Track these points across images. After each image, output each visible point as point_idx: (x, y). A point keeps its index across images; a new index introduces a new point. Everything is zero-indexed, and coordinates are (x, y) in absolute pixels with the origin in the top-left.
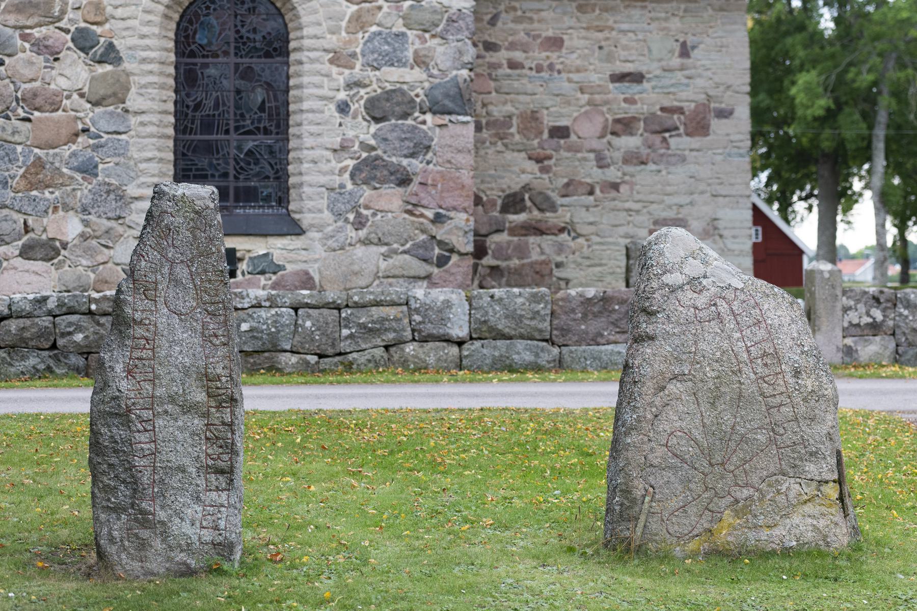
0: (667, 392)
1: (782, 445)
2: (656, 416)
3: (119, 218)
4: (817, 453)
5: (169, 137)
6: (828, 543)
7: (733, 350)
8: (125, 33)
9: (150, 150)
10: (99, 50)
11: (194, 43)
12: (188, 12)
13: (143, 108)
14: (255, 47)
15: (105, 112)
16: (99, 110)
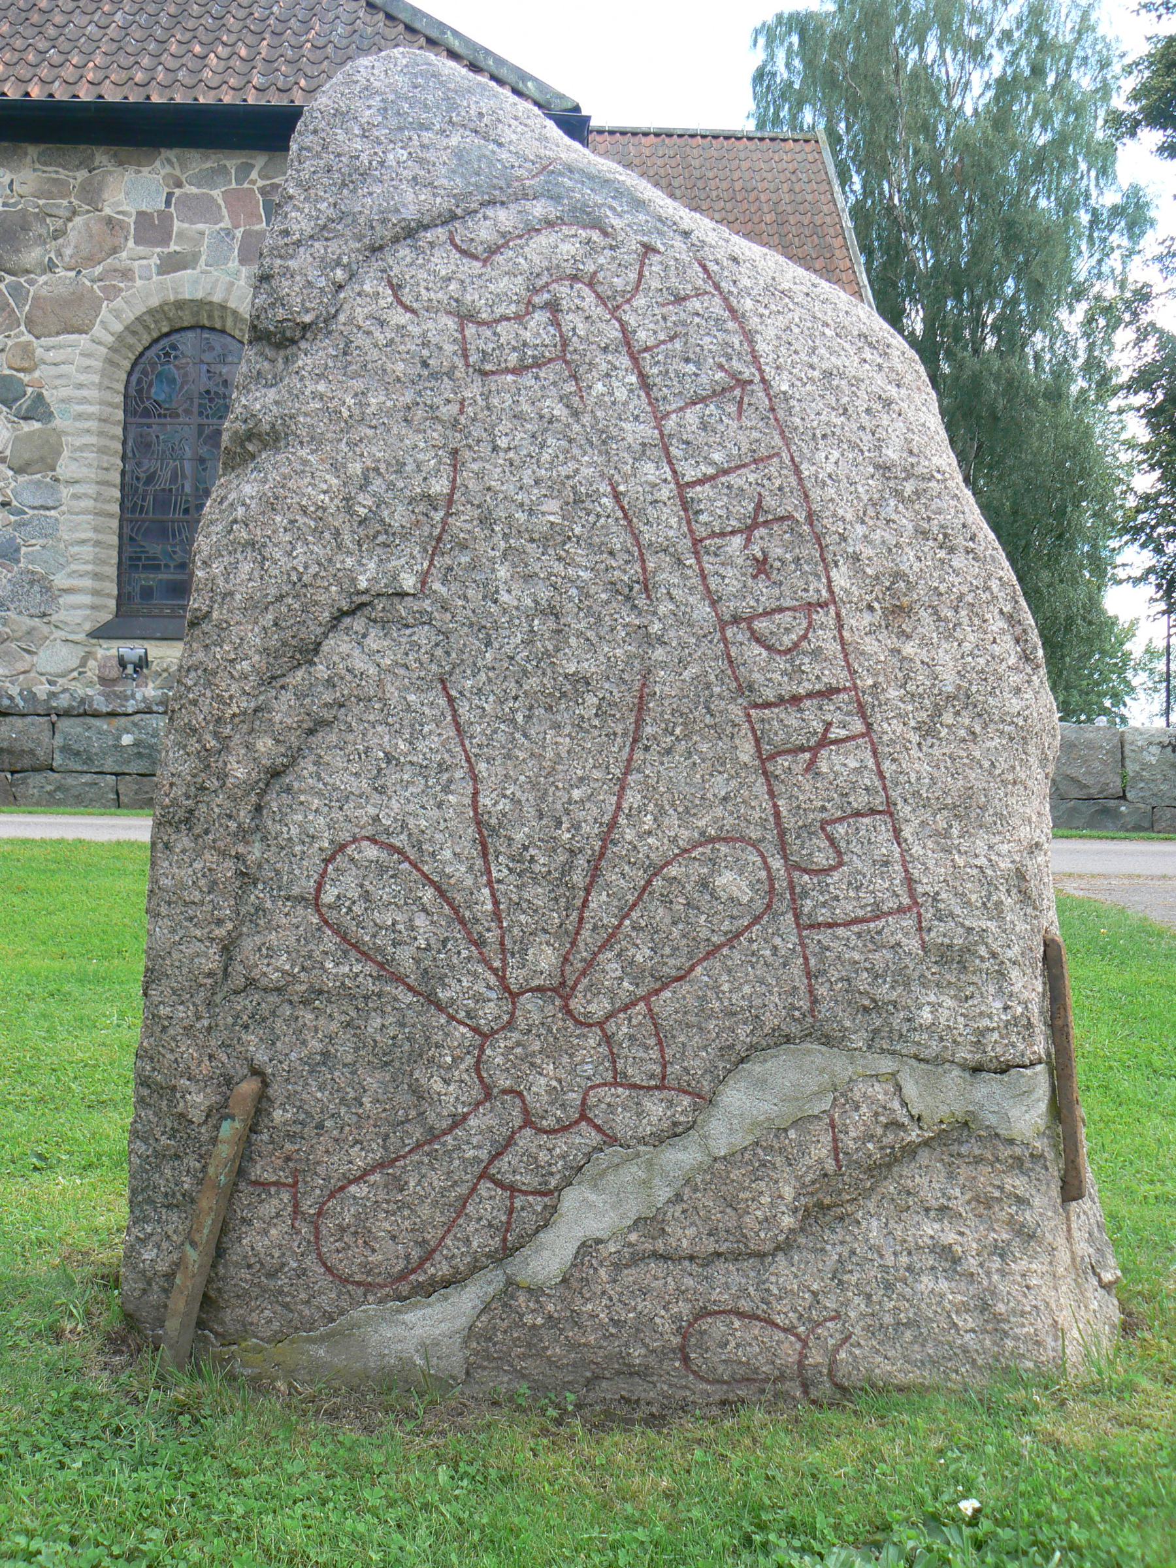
0: (321, 671)
1: (823, 915)
2: (275, 774)
3: (45, 615)
4: (968, 950)
5: (112, 516)
6: (997, 1318)
7: (617, 496)
8: (58, 382)
9: (85, 531)
10: (24, 403)
11: (148, 398)
12: (142, 360)
13: (77, 476)
16: (22, 479)
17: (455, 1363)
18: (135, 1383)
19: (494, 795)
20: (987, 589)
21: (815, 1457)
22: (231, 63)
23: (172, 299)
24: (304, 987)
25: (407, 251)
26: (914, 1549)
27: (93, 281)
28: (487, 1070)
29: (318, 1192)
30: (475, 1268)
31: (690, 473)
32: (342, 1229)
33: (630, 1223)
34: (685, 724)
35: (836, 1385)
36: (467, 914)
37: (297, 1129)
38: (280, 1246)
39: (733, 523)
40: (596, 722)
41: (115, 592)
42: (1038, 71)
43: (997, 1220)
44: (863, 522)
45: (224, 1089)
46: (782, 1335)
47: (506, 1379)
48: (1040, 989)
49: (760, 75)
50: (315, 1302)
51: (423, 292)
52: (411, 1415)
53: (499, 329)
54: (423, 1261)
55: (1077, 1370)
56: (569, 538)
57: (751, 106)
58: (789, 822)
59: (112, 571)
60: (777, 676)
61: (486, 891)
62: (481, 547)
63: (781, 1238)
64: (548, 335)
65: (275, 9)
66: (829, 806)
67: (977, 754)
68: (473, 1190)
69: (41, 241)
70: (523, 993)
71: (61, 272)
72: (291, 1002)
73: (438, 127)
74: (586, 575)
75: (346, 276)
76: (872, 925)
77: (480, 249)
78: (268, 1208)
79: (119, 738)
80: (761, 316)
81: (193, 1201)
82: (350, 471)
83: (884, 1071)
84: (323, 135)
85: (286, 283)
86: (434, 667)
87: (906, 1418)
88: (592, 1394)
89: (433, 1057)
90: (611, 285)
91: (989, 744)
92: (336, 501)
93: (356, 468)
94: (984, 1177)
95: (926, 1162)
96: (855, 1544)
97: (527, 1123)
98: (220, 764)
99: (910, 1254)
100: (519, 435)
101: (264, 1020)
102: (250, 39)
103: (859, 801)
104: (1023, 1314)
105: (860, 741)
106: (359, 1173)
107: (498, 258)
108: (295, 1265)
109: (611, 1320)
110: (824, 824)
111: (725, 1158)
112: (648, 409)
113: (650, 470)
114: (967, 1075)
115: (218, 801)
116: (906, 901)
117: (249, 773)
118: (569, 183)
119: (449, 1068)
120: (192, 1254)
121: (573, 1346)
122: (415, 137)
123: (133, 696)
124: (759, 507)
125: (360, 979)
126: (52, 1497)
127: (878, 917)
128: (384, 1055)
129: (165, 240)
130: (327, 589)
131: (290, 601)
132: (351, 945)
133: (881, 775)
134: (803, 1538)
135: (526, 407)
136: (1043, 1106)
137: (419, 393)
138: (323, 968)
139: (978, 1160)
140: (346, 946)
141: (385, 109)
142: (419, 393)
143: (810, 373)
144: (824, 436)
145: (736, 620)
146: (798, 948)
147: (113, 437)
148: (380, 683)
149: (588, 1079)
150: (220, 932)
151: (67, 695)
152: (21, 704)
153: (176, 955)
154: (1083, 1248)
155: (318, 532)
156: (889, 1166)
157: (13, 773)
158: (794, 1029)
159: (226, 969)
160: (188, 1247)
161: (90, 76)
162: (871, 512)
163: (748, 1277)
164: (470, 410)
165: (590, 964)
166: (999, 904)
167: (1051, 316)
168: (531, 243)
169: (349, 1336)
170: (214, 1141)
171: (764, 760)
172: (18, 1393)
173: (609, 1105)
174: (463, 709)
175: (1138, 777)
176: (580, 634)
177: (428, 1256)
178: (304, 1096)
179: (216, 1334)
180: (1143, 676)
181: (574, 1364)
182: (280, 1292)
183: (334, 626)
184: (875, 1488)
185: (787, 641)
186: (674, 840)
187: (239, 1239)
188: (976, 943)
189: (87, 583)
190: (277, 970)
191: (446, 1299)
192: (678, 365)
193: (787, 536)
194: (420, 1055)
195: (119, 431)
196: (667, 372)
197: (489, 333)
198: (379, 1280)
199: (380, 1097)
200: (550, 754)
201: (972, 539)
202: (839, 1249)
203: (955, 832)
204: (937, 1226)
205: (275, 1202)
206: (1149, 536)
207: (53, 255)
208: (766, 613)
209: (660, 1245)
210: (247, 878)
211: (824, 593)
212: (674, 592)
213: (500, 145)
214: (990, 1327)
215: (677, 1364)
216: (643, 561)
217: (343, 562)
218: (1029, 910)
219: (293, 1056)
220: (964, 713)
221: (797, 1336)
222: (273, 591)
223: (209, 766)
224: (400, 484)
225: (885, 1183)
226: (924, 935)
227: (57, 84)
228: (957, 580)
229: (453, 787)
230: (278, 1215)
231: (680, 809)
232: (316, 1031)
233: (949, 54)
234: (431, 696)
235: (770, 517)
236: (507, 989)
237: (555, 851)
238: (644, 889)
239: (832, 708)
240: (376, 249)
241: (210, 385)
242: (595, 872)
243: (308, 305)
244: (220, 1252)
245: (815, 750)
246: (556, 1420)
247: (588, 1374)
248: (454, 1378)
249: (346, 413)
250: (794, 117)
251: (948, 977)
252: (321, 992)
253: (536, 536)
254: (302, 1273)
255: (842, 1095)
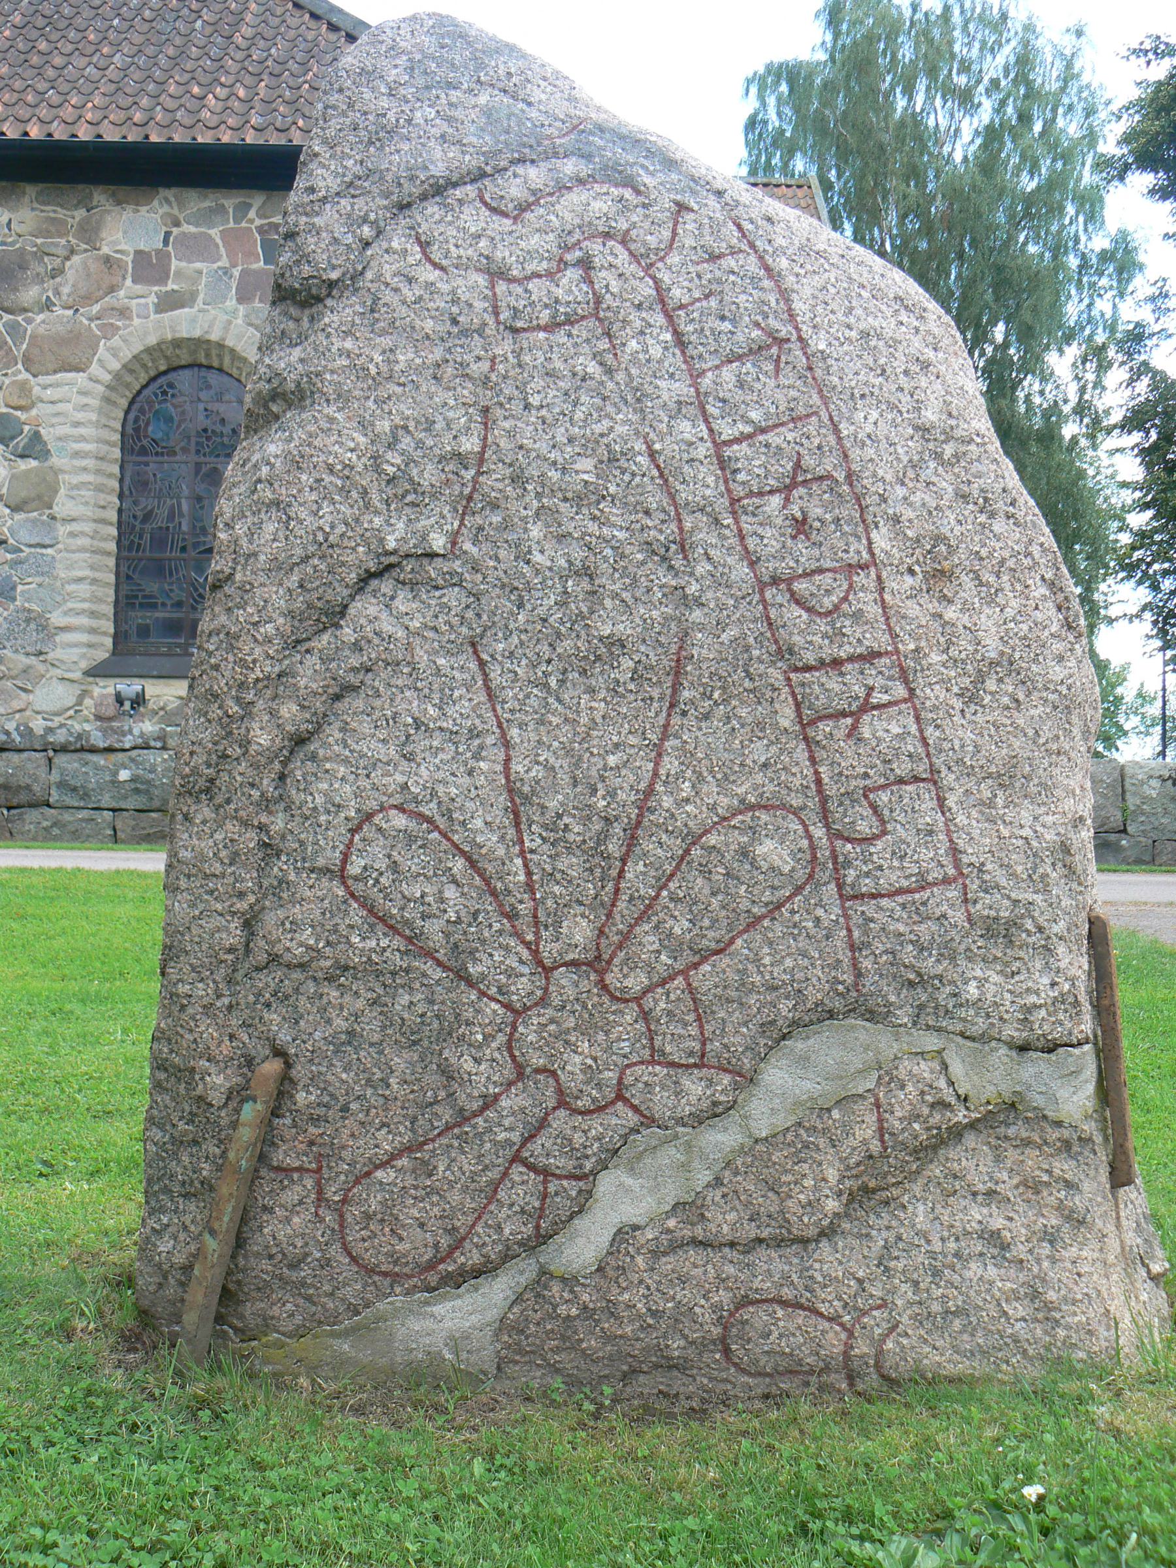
0: (348, 633)
1: (867, 885)
2: (300, 740)
3: (41, 653)
4: (1013, 924)
5: (109, 554)
6: (1048, 1307)
7: (652, 454)
8: (54, 420)
9: (81, 568)
10: (21, 441)
11: (146, 437)
13: (74, 514)
14: (223, 444)
15: (27, 520)
17: (485, 1355)
18: (151, 1379)
19: (526, 762)
20: (1028, 554)
21: (865, 1447)
22: (230, 103)
23: (169, 337)
24: (328, 963)
25: (436, 208)
26: (978, 1536)
27: (91, 319)
28: (520, 1049)
29: (343, 1177)
30: (507, 1257)
31: (727, 431)
32: (368, 1217)
33: (668, 1208)
34: (723, 688)
35: (883, 1376)
36: (499, 885)
37: (321, 1111)
38: (303, 1235)
39: (771, 482)
40: (632, 686)
41: (112, 631)
42: (1025, 118)
43: (1046, 1206)
44: (903, 484)
45: (245, 1070)
46: (827, 1325)
47: (538, 1374)
48: (1086, 967)
49: (752, 123)
50: (339, 1294)
51: (453, 249)
52: (441, 1410)
53: (530, 286)
54: (452, 1249)
55: (1133, 1362)
56: (604, 497)
57: (743, 153)
58: (831, 790)
59: (109, 610)
60: (817, 639)
61: (519, 861)
62: (514, 506)
63: (825, 1223)
64: (581, 292)
65: (273, 51)
66: (871, 772)
67: (1021, 722)
68: (505, 1174)
69: (39, 279)
70: (557, 968)
71: (58, 310)
72: (315, 979)
73: (465, 86)
74: (621, 535)
75: (373, 233)
76: (917, 896)
77: (511, 206)
78: (291, 1196)
79: (116, 774)
80: (797, 275)
81: (212, 1189)
82: (378, 429)
83: (930, 1048)
84: (348, 93)
85: (311, 240)
86: (464, 630)
87: (958, 1408)
88: (628, 1389)
89: (464, 1035)
90: (644, 243)
91: (1032, 712)
92: (364, 460)
93: (384, 426)
94: (1032, 1160)
95: (973, 1145)
96: (915, 1532)
97: (562, 1103)
98: (243, 731)
99: (957, 1239)
100: (552, 393)
101: (287, 997)
102: (248, 80)
103: (902, 768)
104: (1074, 1302)
105: (903, 706)
106: (386, 1158)
107: (528, 215)
108: (318, 1255)
109: (649, 1310)
110: (867, 791)
111: (766, 1139)
112: (684, 367)
113: (686, 428)
114: (1014, 1054)
115: (241, 769)
116: (951, 871)
117: (273, 740)
118: (600, 143)
119: (480, 1046)
120: (211, 1244)
121: (608, 1338)
122: (443, 96)
123: (130, 732)
124: (798, 466)
125: (387, 954)
126: (68, 1489)
127: (923, 888)
128: (413, 1033)
129: (163, 279)
130: (353, 549)
131: (316, 562)
132: (378, 918)
133: (924, 741)
134: (861, 1525)
135: (558, 364)
136: (1091, 1088)
137: (449, 350)
138: (349, 942)
139: (1027, 1143)
140: (373, 920)
141: (412, 69)
142: (449, 350)
143: (847, 333)
144: (863, 396)
145: (775, 581)
146: (841, 920)
147: (110, 475)
148: (409, 647)
149: (625, 1056)
150: (242, 906)
151: (64, 730)
152: (18, 739)
153: (195, 930)
154: (1132, 1239)
155: (345, 491)
156: (935, 1148)
157: (9, 808)
158: (838, 1004)
159: (247, 945)
160: (207, 1236)
161: (89, 116)
162: (911, 474)
163: (791, 1264)
164: (501, 368)
165: (626, 936)
166: (1044, 876)
167: (1039, 359)
168: (562, 201)
169: (375, 1329)
170: (234, 1125)
171: (805, 724)
172: (30, 1389)
173: (646, 1084)
174: (495, 673)
175: (1139, 811)
176: (615, 596)
177: (458, 1245)
178: (329, 1077)
179: (236, 1330)
180: (1135, 721)
181: (611, 1358)
182: (303, 1284)
183: (361, 589)
184: (932, 1476)
185: (828, 602)
186: (713, 808)
187: (261, 1228)
188: (1022, 917)
189: (84, 621)
190: (301, 945)
191: (477, 1290)
192: (713, 323)
193: (826, 496)
194: (450, 1034)
195: (116, 470)
196: (702, 330)
197: (520, 290)
198: (406, 1270)
199: (408, 1078)
200: (584, 720)
201: (1013, 504)
202: (884, 1234)
203: (1000, 801)
204: (985, 1211)
205: (298, 1188)
206: (1145, 573)
207: (50, 294)
208: (806, 575)
209: (699, 1231)
210: (270, 849)
211: (865, 555)
212: (712, 552)
213: (530, 104)
214: (1040, 1316)
215: (717, 1356)
216: (680, 521)
217: (371, 522)
218: (1074, 885)
219: (318, 1035)
220: (1006, 680)
221: (842, 1325)
222: (298, 552)
223: (231, 733)
224: (430, 442)
225: (931, 1167)
226: (970, 907)
227: (56, 123)
228: (998, 545)
229: (484, 754)
230: (301, 1203)
231: (719, 776)
232: (342, 1009)
233: (938, 102)
234: (462, 659)
235: (809, 476)
236: (540, 963)
237: (590, 819)
238: (682, 858)
239: (874, 672)
240: (404, 207)
241: (207, 423)
242: (632, 841)
243: (334, 261)
244: (240, 1242)
245: (857, 715)
246: (593, 1414)
247: (625, 1368)
248: (485, 1373)
249: (373, 371)
250: (786, 165)
251: (994, 951)
252: (346, 968)
253: (570, 495)
254: (325, 1263)
255: (887, 1073)
